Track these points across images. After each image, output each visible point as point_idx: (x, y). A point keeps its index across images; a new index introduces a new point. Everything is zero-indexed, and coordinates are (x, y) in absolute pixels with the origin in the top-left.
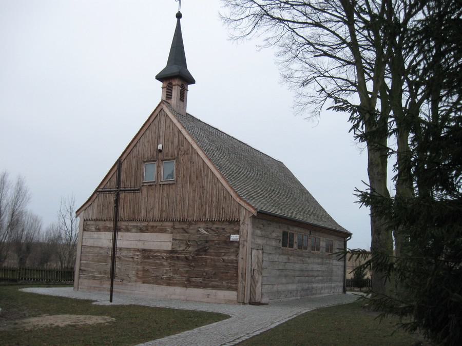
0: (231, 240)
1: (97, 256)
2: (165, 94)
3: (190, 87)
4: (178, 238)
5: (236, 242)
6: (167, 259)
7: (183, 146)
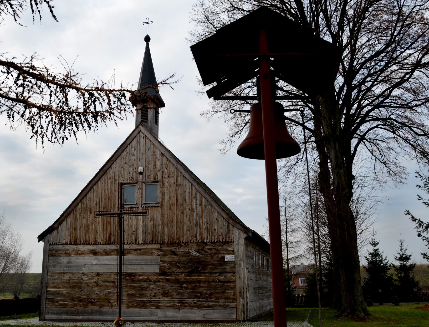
0: (226, 260)
1: (69, 282)
2: (139, 116)
3: (161, 110)
4: (166, 260)
6: (155, 282)
7: (167, 169)
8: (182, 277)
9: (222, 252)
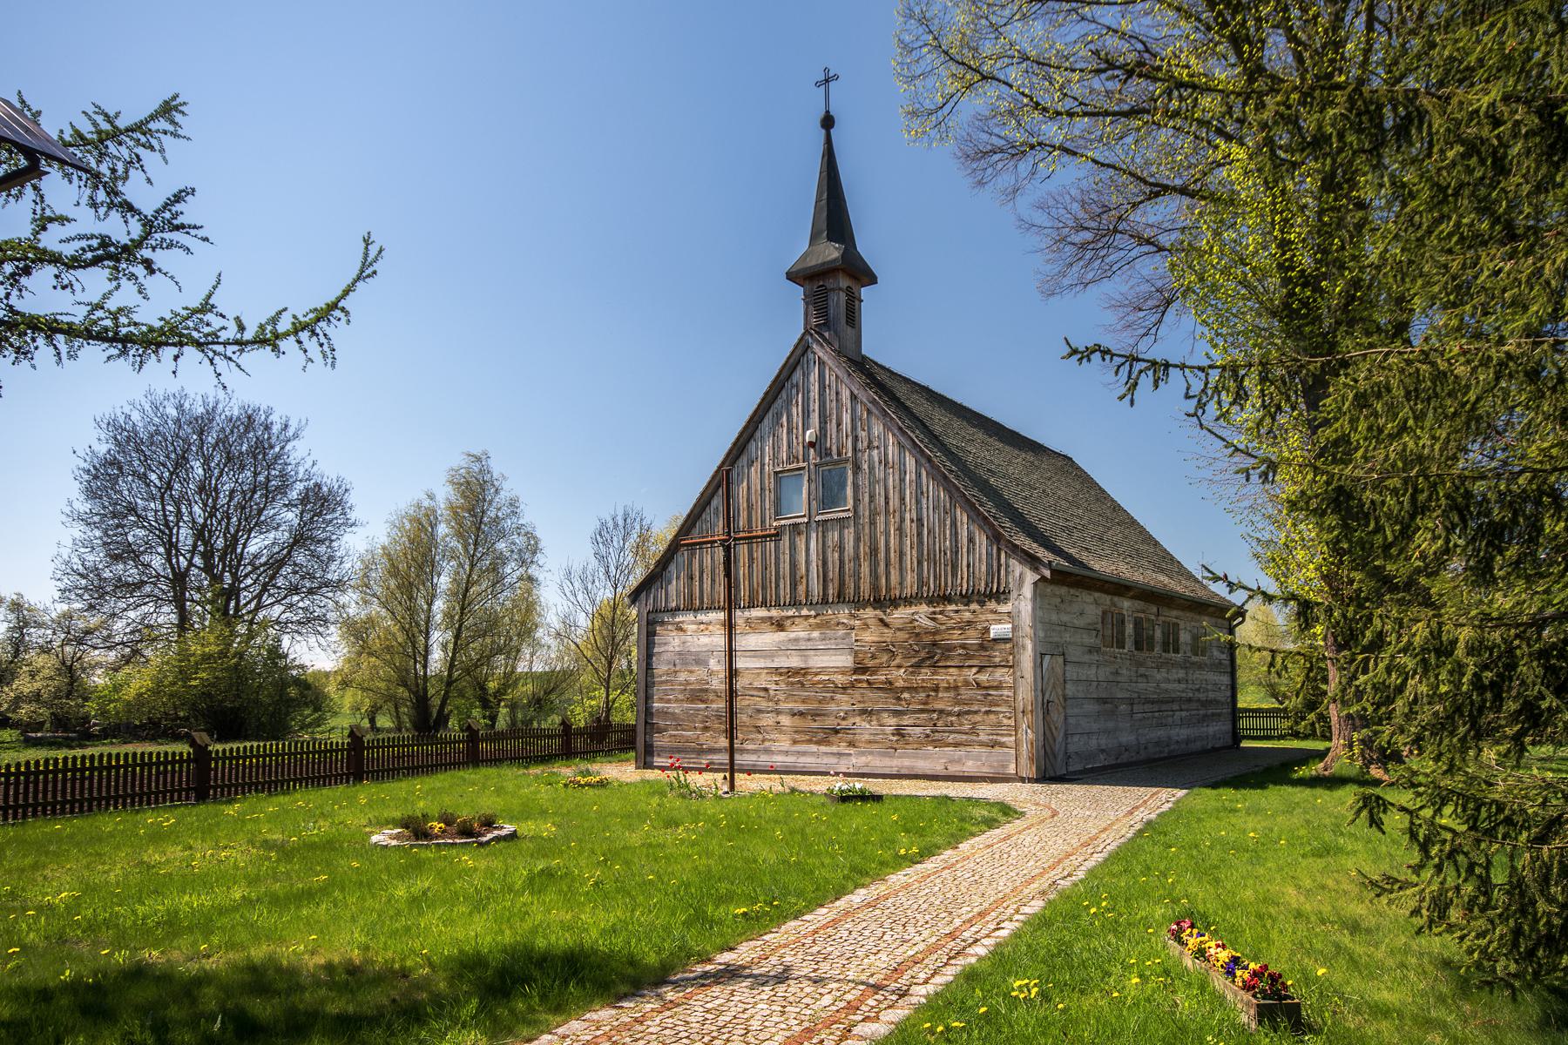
3: (865, 292)
5: (1006, 640)
8: (899, 676)
9: (983, 618)
